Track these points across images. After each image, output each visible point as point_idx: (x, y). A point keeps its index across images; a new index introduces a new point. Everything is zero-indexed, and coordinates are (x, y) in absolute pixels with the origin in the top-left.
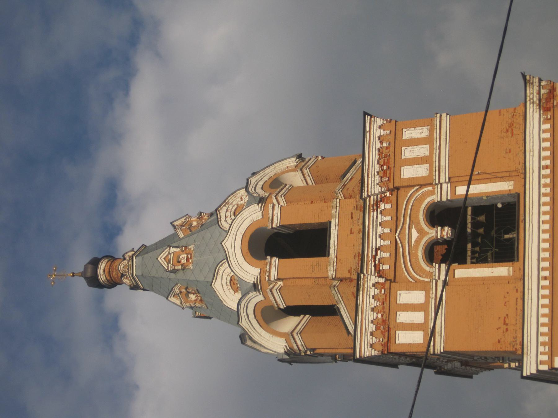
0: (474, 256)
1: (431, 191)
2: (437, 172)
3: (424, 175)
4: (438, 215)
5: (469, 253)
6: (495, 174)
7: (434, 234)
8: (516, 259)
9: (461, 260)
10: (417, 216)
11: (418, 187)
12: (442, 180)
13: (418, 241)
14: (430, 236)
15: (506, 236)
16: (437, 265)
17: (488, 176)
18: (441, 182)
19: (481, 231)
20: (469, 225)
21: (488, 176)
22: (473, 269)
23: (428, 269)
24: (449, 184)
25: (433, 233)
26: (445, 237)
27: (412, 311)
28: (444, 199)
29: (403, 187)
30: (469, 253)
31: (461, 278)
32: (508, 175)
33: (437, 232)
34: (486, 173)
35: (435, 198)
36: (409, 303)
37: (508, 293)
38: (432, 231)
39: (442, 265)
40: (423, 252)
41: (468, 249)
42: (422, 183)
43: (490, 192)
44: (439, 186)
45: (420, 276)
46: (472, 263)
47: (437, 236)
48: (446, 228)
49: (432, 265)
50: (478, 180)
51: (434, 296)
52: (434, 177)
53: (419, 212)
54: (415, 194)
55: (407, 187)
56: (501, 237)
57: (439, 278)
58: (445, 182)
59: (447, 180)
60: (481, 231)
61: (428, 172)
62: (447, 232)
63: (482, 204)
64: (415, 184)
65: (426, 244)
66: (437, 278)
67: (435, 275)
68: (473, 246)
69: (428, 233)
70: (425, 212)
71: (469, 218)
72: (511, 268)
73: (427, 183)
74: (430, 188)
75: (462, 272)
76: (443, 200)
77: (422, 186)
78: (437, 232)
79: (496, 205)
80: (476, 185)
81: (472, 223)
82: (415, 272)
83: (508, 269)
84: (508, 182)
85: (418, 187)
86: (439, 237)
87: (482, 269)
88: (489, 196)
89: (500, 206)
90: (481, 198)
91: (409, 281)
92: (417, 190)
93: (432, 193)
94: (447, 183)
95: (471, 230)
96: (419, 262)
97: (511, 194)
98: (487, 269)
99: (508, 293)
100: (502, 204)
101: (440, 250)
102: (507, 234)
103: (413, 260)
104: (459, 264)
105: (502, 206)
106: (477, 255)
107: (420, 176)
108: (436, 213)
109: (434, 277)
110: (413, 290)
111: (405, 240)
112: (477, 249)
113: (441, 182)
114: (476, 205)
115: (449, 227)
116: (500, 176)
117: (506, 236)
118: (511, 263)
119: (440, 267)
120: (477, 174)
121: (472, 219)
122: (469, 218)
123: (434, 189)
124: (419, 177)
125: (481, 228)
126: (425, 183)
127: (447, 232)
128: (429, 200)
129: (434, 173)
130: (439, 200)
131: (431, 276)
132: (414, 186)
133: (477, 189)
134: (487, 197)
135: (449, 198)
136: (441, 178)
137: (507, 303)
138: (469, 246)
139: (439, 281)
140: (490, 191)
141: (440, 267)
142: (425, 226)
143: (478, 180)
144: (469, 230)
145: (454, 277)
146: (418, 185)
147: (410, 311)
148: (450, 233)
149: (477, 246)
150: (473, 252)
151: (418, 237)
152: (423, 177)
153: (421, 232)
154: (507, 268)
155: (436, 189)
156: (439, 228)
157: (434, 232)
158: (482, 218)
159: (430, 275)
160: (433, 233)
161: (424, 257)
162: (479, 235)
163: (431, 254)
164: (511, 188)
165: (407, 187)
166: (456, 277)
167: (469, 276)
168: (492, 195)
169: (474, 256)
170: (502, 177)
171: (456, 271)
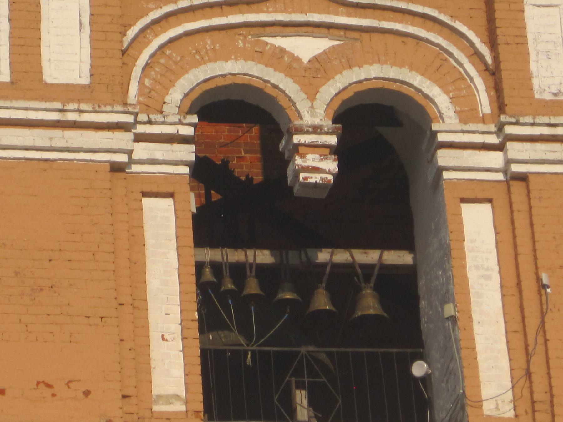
0: (226, 273)
1: (474, 109)
2: (546, 131)
3: (535, 82)
4: (383, 136)
5: (236, 256)
6: (540, 348)
7: (308, 119)
8: (228, 265)
9: (206, 228)
10: (377, 58)
11: (489, 60)
12: (516, 150)
13: (282, 60)
14: (303, 105)
15: (301, 397)
16: (189, 131)
17: (533, 323)
18: (510, 145)
19: (322, 301)
20: (342, 257)
21: (533, 323)
22: (176, 264)
23: (175, 96)
24: (500, 177)
25: (312, 114)
26: (298, 161)
27: (11, 36)
28: (444, 158)
29: (528, 186)
30: (236, 256)
31: (140, 218)
32: (537, 396)
33: (316, 130)
34: (543, 315)
35: (447, 123)
36: (44, 26)
37: (87, 393)
38: (321, 109)
39: (192, 148)
40: (239, 80)
41: (250, 253)
42: (504, 74)
43: (469, 328)
44: (493, 139)
45: (147, 66)
46: (199, 267)
47: (300, 131)
48: (331, 165)
49: (190, 112)
50: (519, 284)
51: (71, 117)
52: (528, 119)
53: (393, 64)
54: (462, 50)
55: (491, 20)
56: (298, 373)
57: (139, 138)
58: (509, 162)
59: (515, 168)
60: (322, 301)
61: (548, 97)
62: (316, 166)
63: (423, 304)
64: (502, 48)
65: (269, 90)
66: (140, 129)
67: (150, 122)
68: (262, 271)
69: (312, 96)
70: (395, 87)
71: (370, 257)
72: (184, 408)
73: (507, 92)
74: (485, 105)
75: (163, 232)
76: (441, 153)
77: (493, 73)
78: (316, 130)
79: (421, 357)
80: (496, 278)
81: (350, 266)
82: (162, 47)
83: (177, 397)
84: (509, 395)
85: (489, 60)
86: (297, 139)
87: (177, 299)
88: (454, 328)
89: (419, 369)
90: (447, 297)
91: (128, 26)
92: (476, 55)
93: (468, 114)
94: (505, 171)
95: (323, 265)
96: (203, 62)
97: (463, 408)
98: (178, 318)
99: (87, 393)
100: (426, 379)
101: (248, 165)
102: (312, 403)
103: (208, 40)
104: (196, 218)
105: (416, 379)
106: (229, 285)
107: (533, 67)
108: (388, 132)
109: (142, 117)
110: (93, 40)
111: (285, 11)
112: (252, 287)
113: (510, 145)
114: (422, 283)
115: (337, 177)
116: (533, 369)
117: (301, 397)
118: (200, 407)
119: (185, 140)
120: (539, 280)
121: (367, 268)
122: (370, 257)
123: (483, 120)
124: (527, 61)
125: (333, 301)
126: (506, 85)
127: (316, 170)
128: (441, 100)
129: (546, 120)
130: (441, 137)
131: (147, 108)
132: (493, 44)
133: (477, 230)
134: (453, 319)
135: (446, 175)
136: (527, 145)
137: (48, 392)
138: (264, 257)
139: (130, 136)
140: (477, 328)
141: (185, 140)
142: (340, 86)
143: (519, 284)
144: (323, 256)
145: (146, 194)
146: (496, 59)
147: (12, 28)
148: (315, 178)
149: (262, 285)
150: (239, 271)
151: (298, 60)
152: (529, 77)
153: (314, 73)
154: (183, 394)
155: (481, 127)
156: (333, 140)
157: (317, 121)
158: (369, 304)
159: (153, 104)
160: (312, 114)
161: (221, 82)
162: (307, 294)
163: (236, 111)
164: (488, 408)
165: (491, 20)
166: (147, 202)
167: (149, 251)
168: (460, 334)
169: (226, 273)
170: (529, 374)
171: (169, 202)
